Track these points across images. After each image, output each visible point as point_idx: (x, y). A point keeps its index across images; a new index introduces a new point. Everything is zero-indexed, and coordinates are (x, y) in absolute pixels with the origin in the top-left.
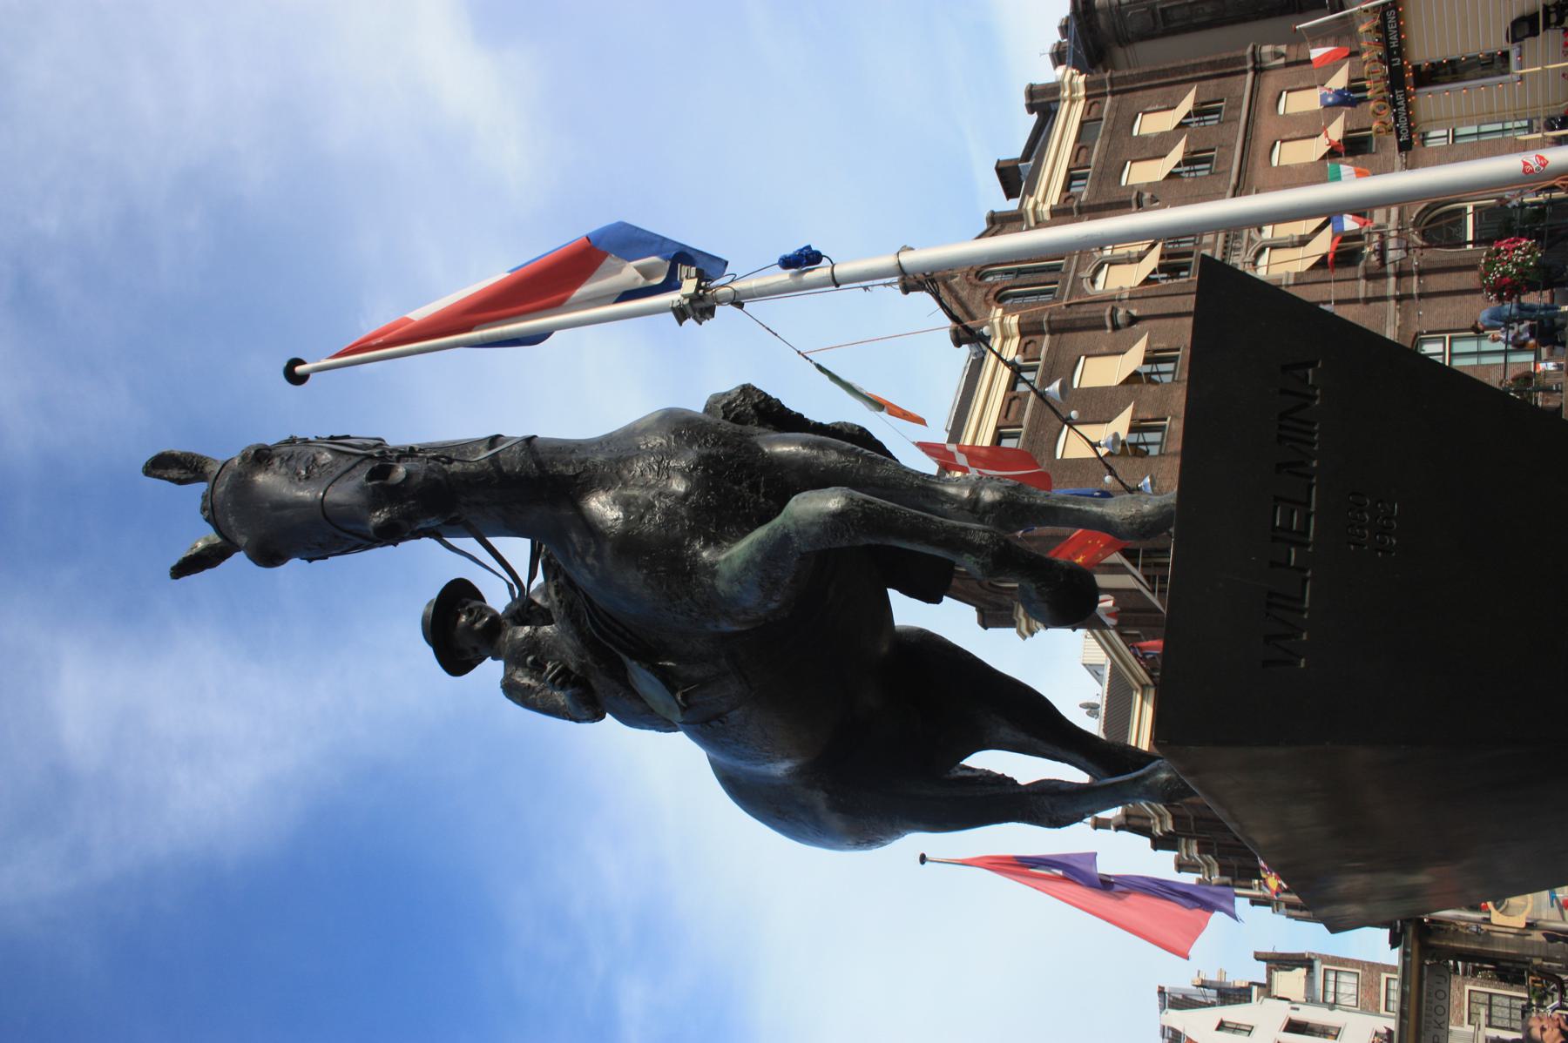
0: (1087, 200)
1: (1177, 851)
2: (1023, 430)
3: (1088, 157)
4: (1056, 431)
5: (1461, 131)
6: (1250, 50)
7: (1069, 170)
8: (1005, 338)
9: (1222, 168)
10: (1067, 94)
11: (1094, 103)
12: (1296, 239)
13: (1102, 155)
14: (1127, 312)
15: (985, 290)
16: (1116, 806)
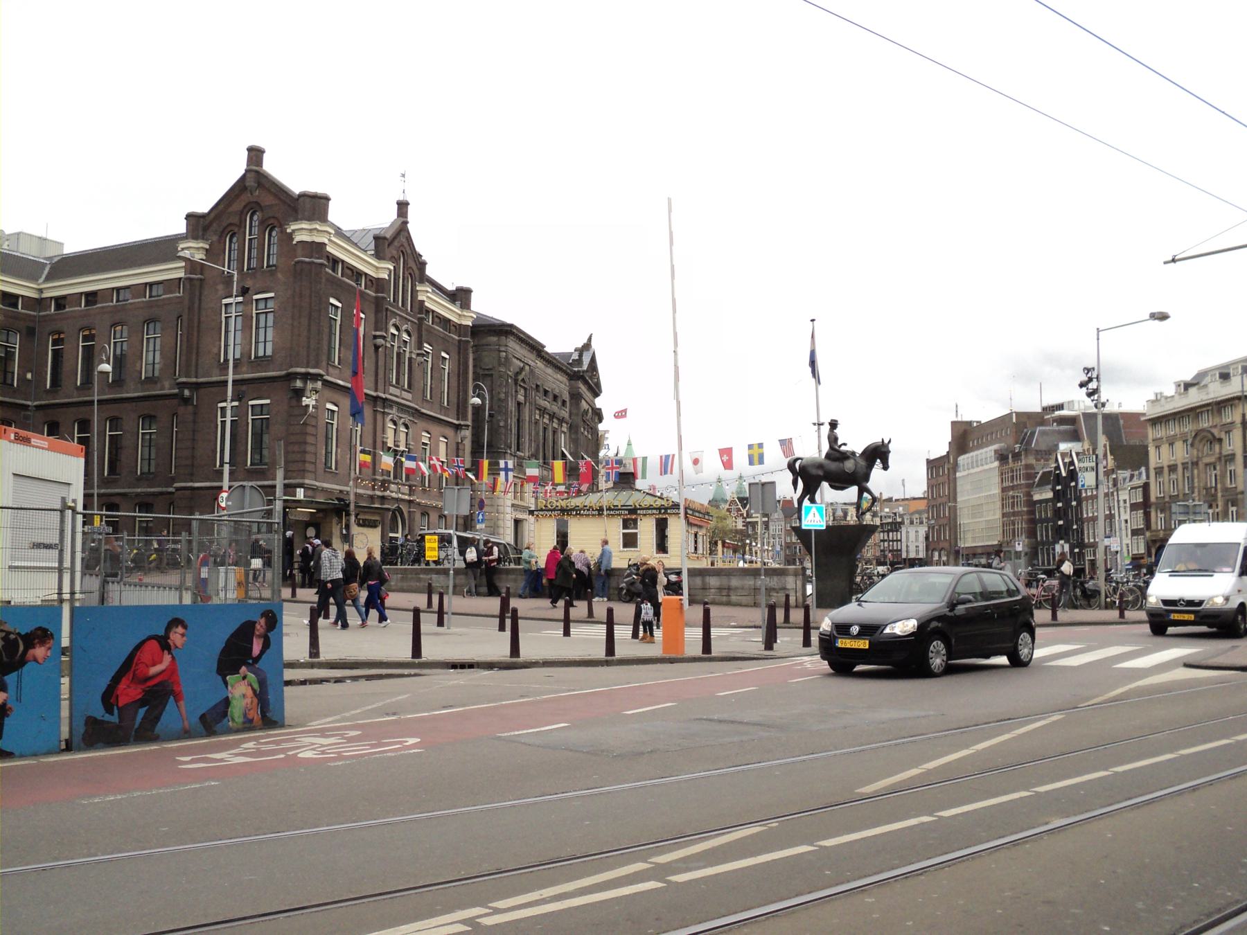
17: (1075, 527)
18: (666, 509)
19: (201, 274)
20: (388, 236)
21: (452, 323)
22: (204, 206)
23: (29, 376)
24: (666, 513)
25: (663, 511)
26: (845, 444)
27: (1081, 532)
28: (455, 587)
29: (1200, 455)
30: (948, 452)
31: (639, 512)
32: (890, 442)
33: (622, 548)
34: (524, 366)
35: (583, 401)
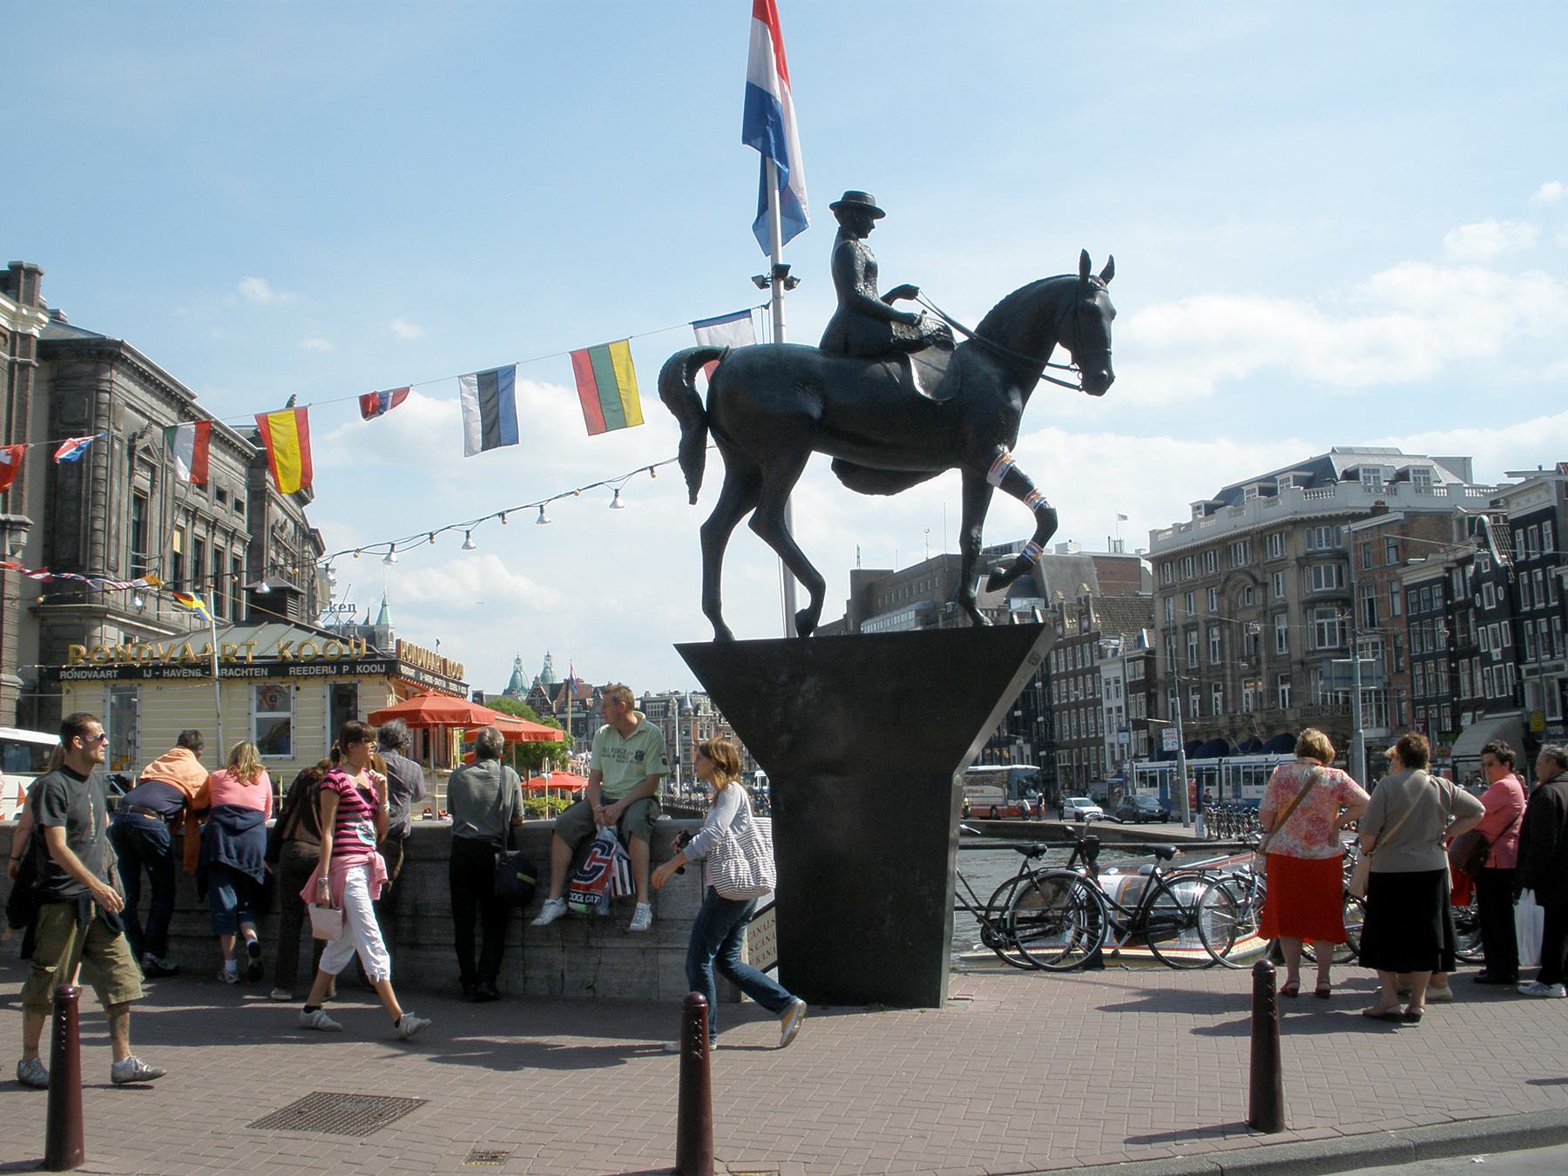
6: (28, 520)
11: (6, 340)
16: (871, 636)
17: (1040, 719)
18: (353, 663)
24: (352, 672)
25: (345, 668)
26: (908, 292)
27: (1050, 724)
28: (1351, 679)
29: (1233, 610)
30: (845, 616)
31: (292, 670)
32: (1108, 273)
34: (149, 426)
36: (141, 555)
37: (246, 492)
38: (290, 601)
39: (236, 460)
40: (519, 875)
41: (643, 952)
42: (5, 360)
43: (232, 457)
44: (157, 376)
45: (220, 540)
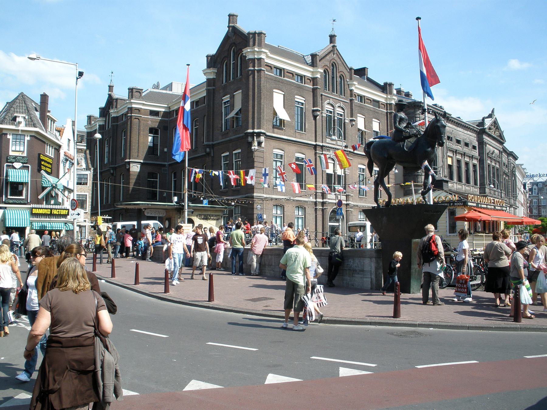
0: (354, 102)
1: (100, 117)
2: (303, 84)
3: (368, 103)
4: (378, 118)
5: (300, 221)
7: (284, 69)
8: (313, 72)
9: (297, 134)
10: (389, 97)
11: (385, 106)
12: (336, 171)
13: (368, 108)
14: (318, 115)
15: (329, 66)
18: (454, 202)
19: (214, 86)
20: (320, 54)
21: (380, 103)
22: (213, 51)
23: (166, 150)
24: (454, 205)
25: (452, 204)
33: (448, 234)
35: (487, 145)
36: (436, 167)
37: (477, 143)
38: (444, 184)
39: (472, 132)
40: (337, 258)
41: (361, 277)
42: (385, 112)
43: (470, 132)
44: (436, 110)
45: (467, 159)
